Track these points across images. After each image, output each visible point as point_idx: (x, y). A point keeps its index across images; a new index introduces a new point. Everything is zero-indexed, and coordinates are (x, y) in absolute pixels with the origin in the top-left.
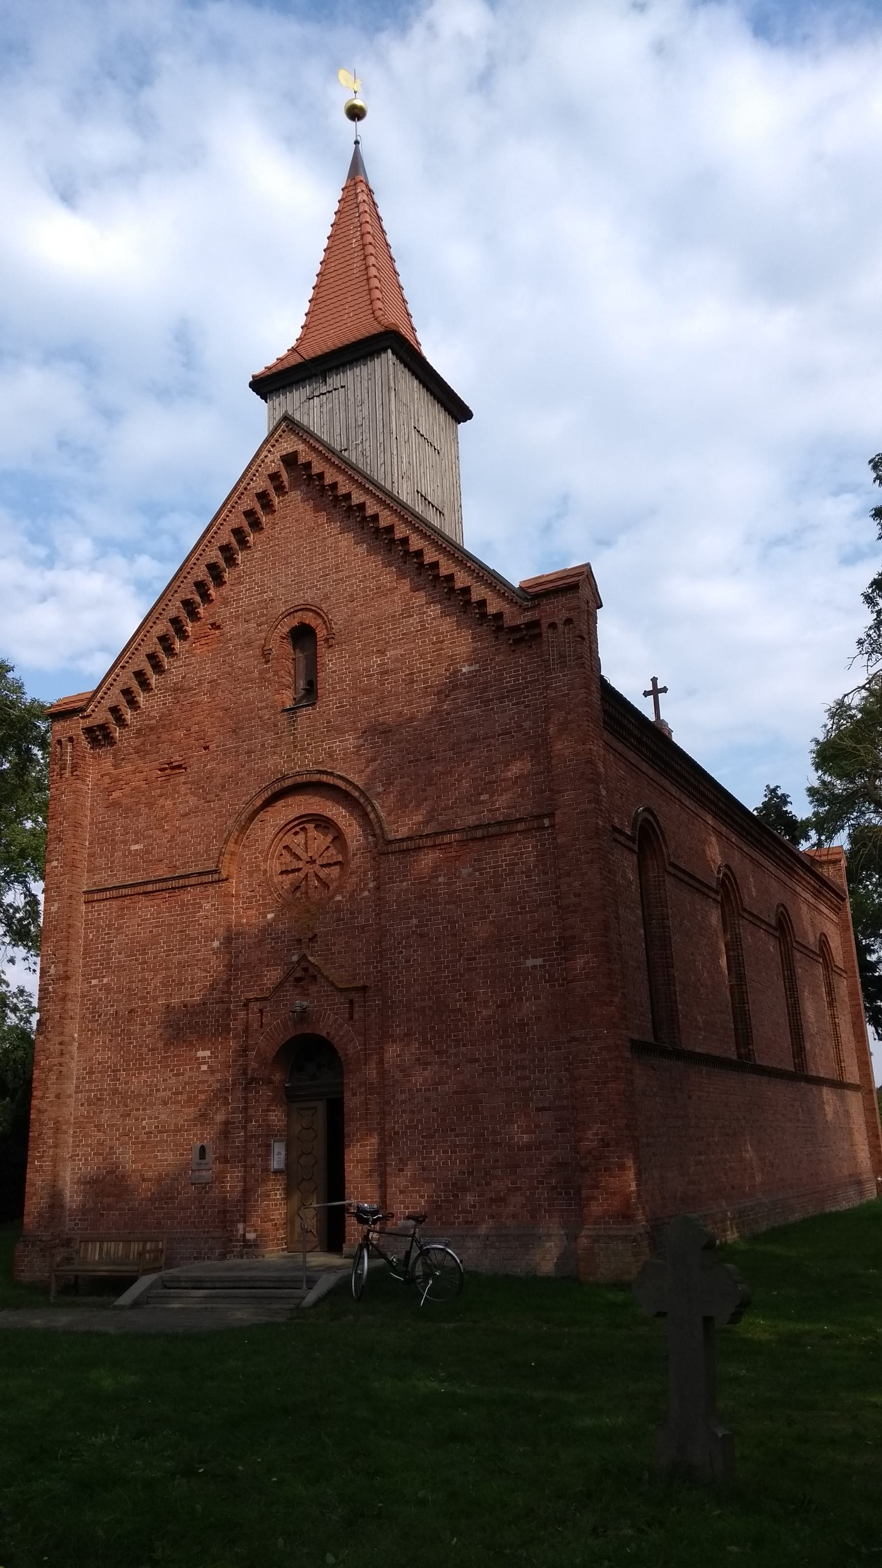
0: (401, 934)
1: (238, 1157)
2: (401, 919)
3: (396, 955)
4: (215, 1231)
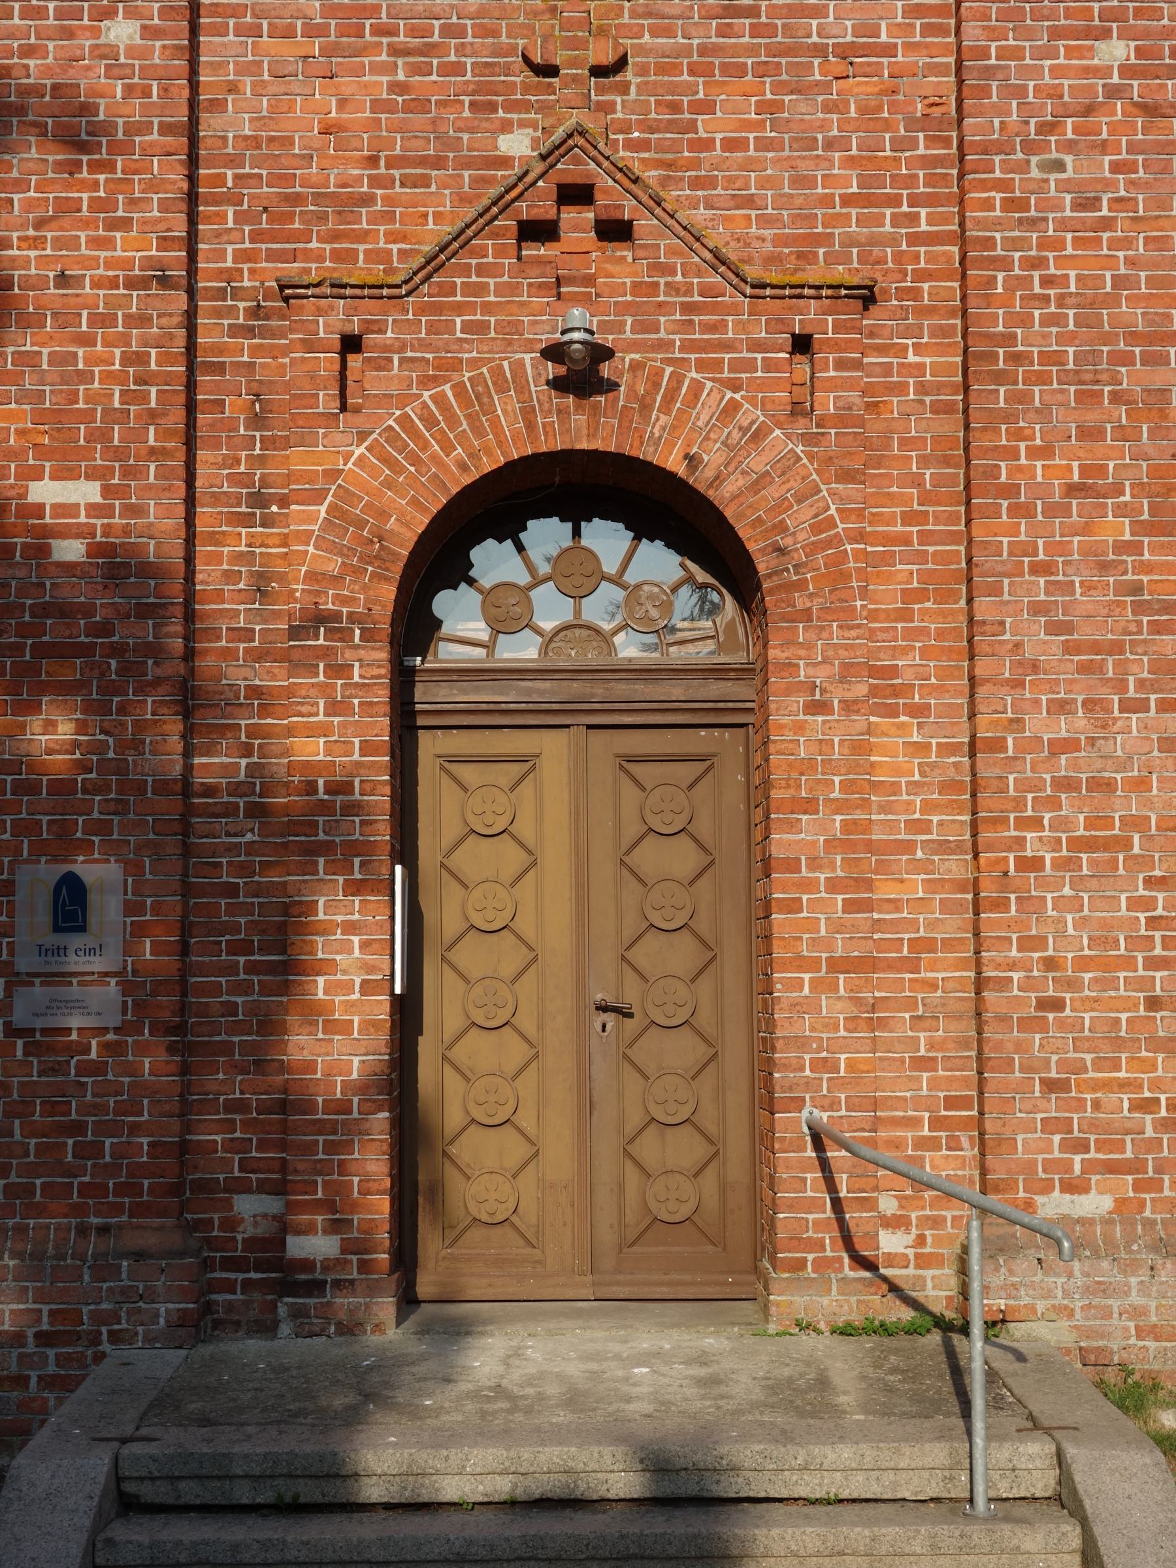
0: (1055, 94)
1: (235, 928)
2: (1056, 34)
3: (1035, 173)
4: (138, 1227)
